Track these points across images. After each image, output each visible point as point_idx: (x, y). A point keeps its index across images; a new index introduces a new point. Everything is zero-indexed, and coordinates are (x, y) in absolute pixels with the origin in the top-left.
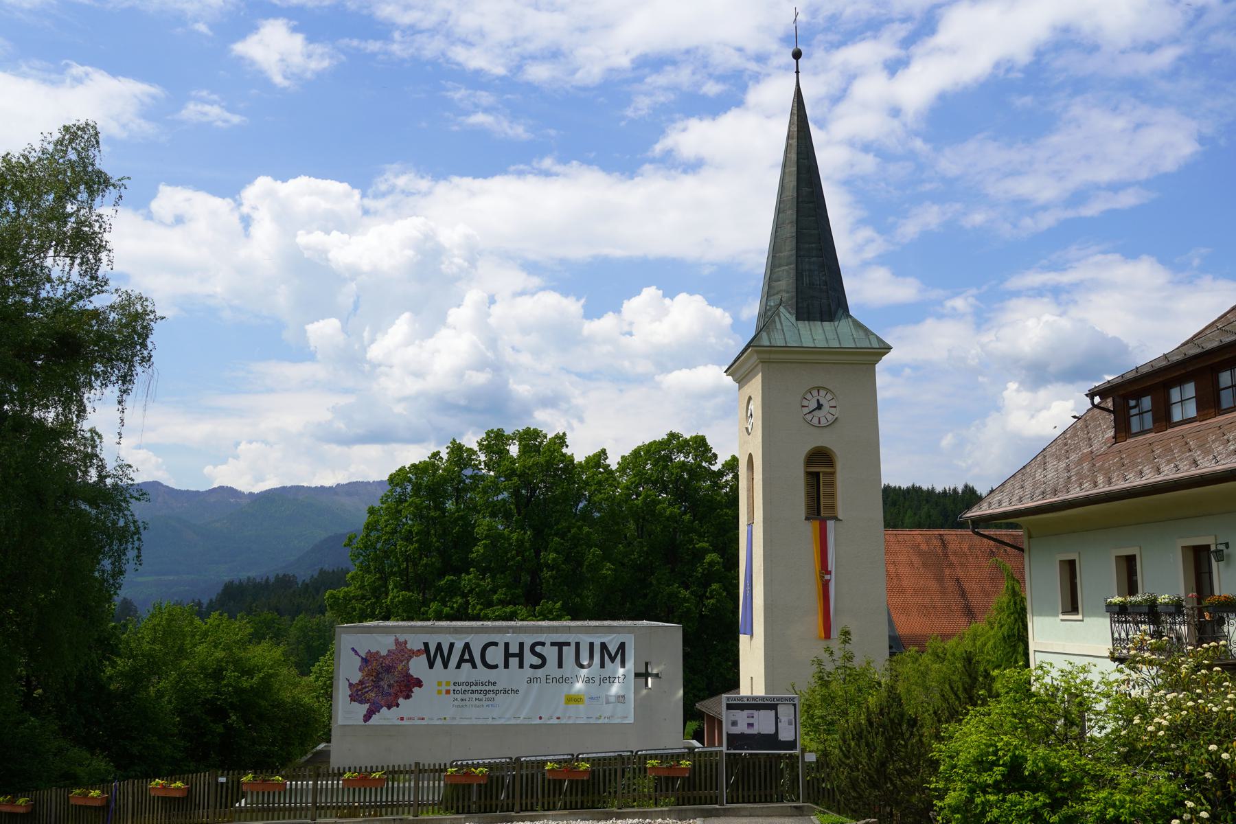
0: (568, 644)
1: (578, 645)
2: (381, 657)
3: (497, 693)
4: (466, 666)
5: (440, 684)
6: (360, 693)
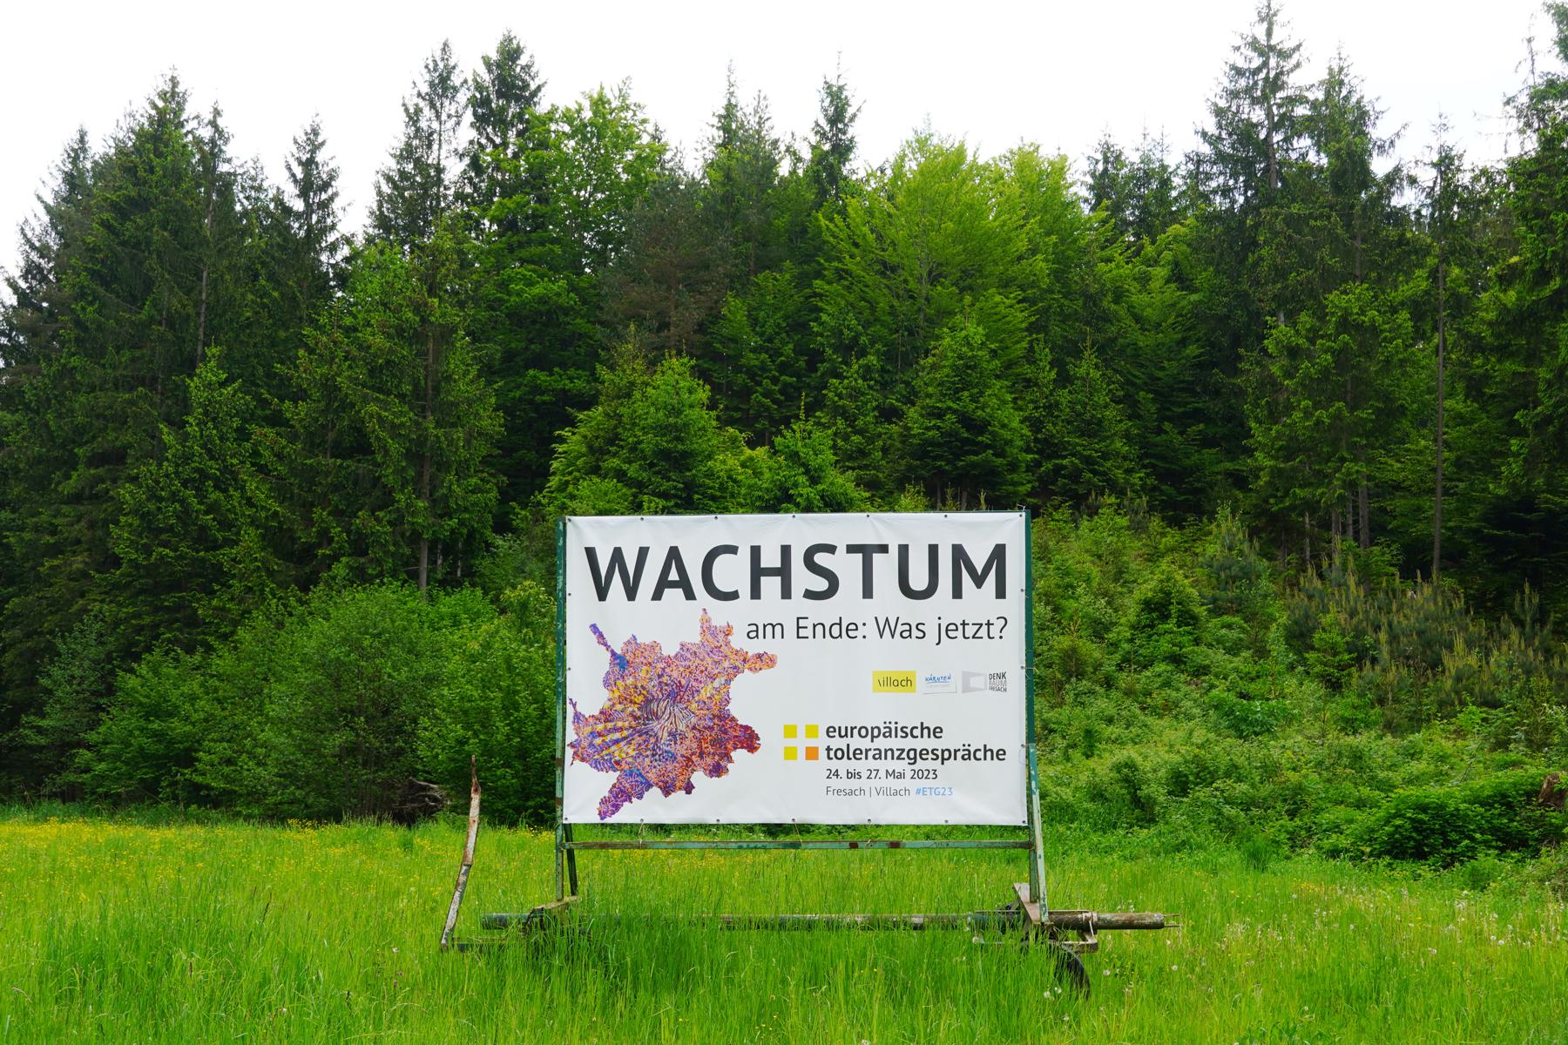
0: (883, 549)
1: (904, 550)
2: (661, 659)
3: (945, 756)
4: (674, 595)
5: (790, 731)
6: (598, 741)
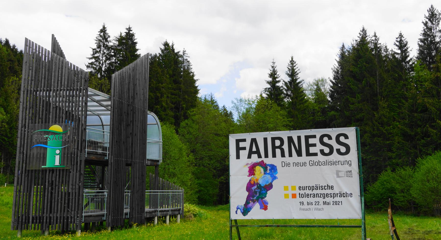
5: (286, 188)
